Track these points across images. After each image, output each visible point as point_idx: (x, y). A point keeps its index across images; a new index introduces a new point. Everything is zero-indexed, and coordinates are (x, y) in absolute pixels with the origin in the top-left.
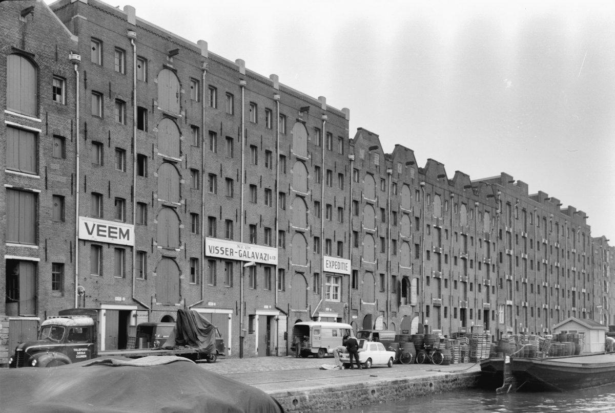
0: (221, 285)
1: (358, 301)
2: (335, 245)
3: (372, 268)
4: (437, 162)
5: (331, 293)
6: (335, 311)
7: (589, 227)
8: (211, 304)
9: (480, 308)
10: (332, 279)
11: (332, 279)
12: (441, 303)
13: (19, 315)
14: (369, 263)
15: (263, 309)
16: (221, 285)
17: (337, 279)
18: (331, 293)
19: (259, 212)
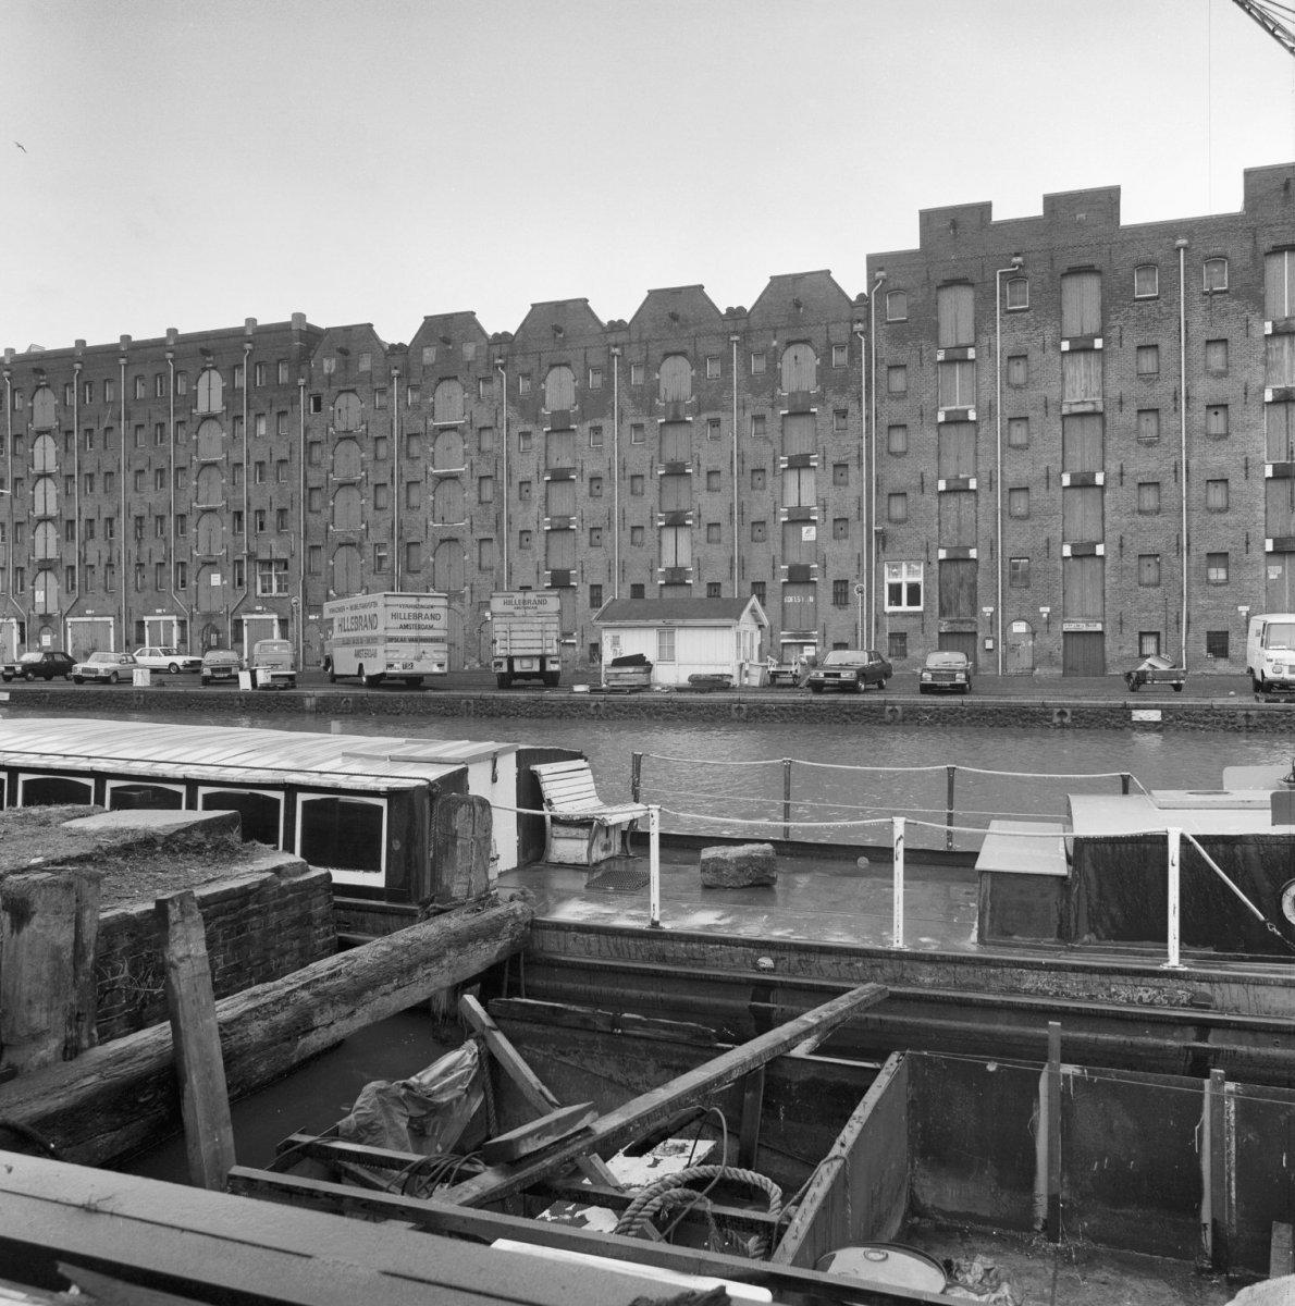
8: (159, 611)
15: (155, 614)
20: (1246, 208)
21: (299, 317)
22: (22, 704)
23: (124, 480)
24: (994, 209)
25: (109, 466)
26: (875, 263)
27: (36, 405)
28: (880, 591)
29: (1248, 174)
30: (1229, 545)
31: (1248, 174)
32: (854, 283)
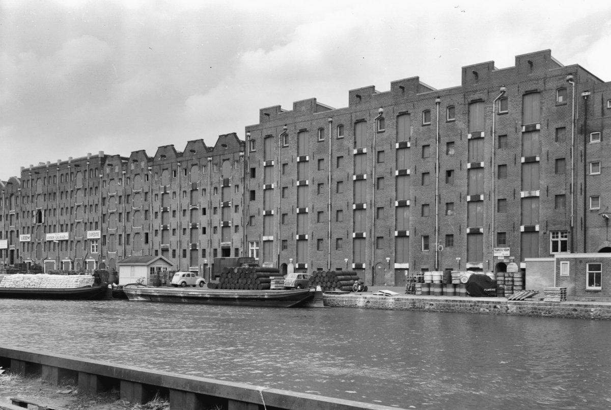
0: (52, 251)
1: (106, 252)
2: (94, 224)
3: (114, 232)
4: (192, 141)
5: (95, 249)
6: (94, 258)
7: (519, 59)
8: (50, 258)
9: (217, 247)
10: (95, 242)
11: (95, 242)
12: (231, 245)
13: (585, 252)
14: (112, 230)
15: (65, 259)
16: (52, 251)
17: (96, 241)
18: (95, 249)
19: (65, 218)
20: (462, 84)
21: (102, 152)
22: (610, 306)
23: (58, 212)
24: (552, 52)
25: (55, 207)
26: (248, 129)
27: (77, 179)
28: (547, 243)
29: (350, 92)
30: (343, 236)
31: (350, 92)
32: (242, 137)
